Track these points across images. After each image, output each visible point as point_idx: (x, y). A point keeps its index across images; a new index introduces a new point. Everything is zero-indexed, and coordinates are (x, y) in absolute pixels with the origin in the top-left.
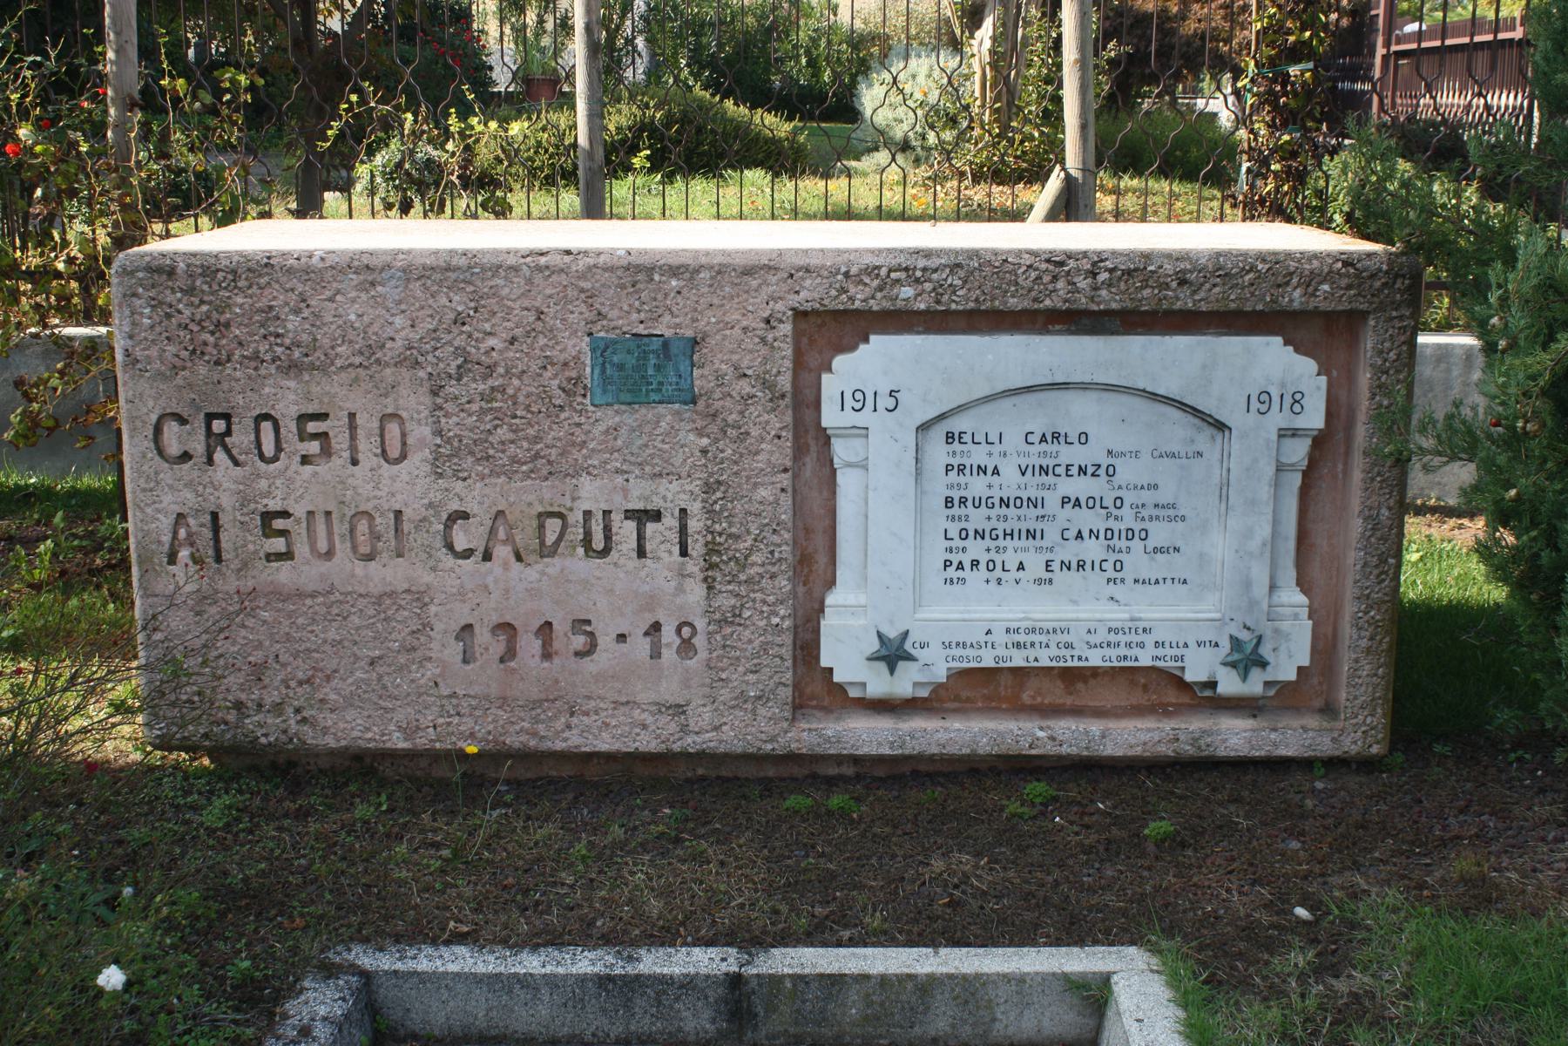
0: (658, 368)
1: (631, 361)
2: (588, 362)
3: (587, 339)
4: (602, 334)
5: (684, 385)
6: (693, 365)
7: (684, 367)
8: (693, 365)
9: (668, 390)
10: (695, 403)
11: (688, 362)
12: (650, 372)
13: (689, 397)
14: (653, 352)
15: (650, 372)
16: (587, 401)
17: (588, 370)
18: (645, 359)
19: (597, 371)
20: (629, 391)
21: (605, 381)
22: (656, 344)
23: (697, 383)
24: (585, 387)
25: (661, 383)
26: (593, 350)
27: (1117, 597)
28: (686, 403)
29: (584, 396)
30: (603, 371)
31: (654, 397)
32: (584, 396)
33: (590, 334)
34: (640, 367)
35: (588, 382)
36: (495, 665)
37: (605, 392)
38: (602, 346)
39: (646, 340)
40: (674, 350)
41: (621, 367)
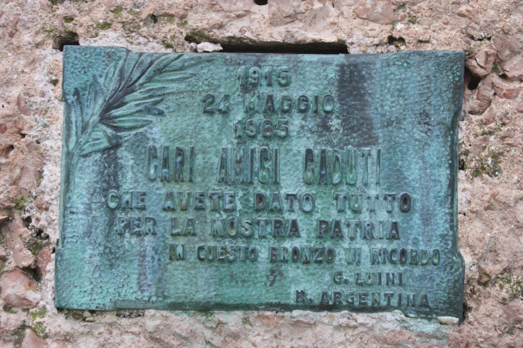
0: (321, 169)
1: (216, 141)
2: (54, 143)
3: (52, 57)
4: (111, 39)
5: (420, 237)
6: (457, 164)
7: (422, 166)
8: (457, 164)
9: (359, 256)
10: (462, 312)
11: (436, 150)
12: (291, 183)
13: (437, 284)
14: (303, 106)
15: (291, 183)
16: (44, 295)
17: (53, 173)
18: (270, 133)
19: (86, 178)
20: (206, 257)
21: (118, 215)
22: (316, 76)
23: (471, 230)
24: (38, 240)
25: (331, 230)
26: (74, 99)
27: (158, 169)
28: (425, 310)
29: (34, 273)
30: (109, 179)
31: (309, 282)
32: (34, 273)
33: (67, 41)
34: (251, 165)
35: (50, 221)
36: (384, 202)
37: (112, 258)
38: (109, 85)
39: (277, 61)
40: (383, 101)
41: (176, 164)
